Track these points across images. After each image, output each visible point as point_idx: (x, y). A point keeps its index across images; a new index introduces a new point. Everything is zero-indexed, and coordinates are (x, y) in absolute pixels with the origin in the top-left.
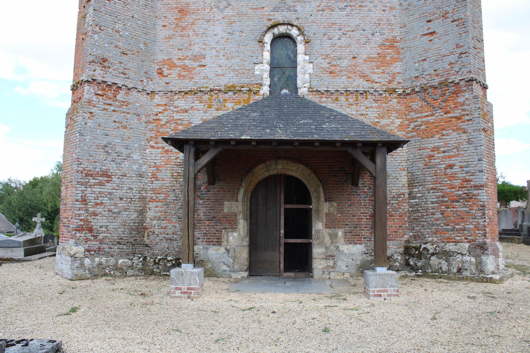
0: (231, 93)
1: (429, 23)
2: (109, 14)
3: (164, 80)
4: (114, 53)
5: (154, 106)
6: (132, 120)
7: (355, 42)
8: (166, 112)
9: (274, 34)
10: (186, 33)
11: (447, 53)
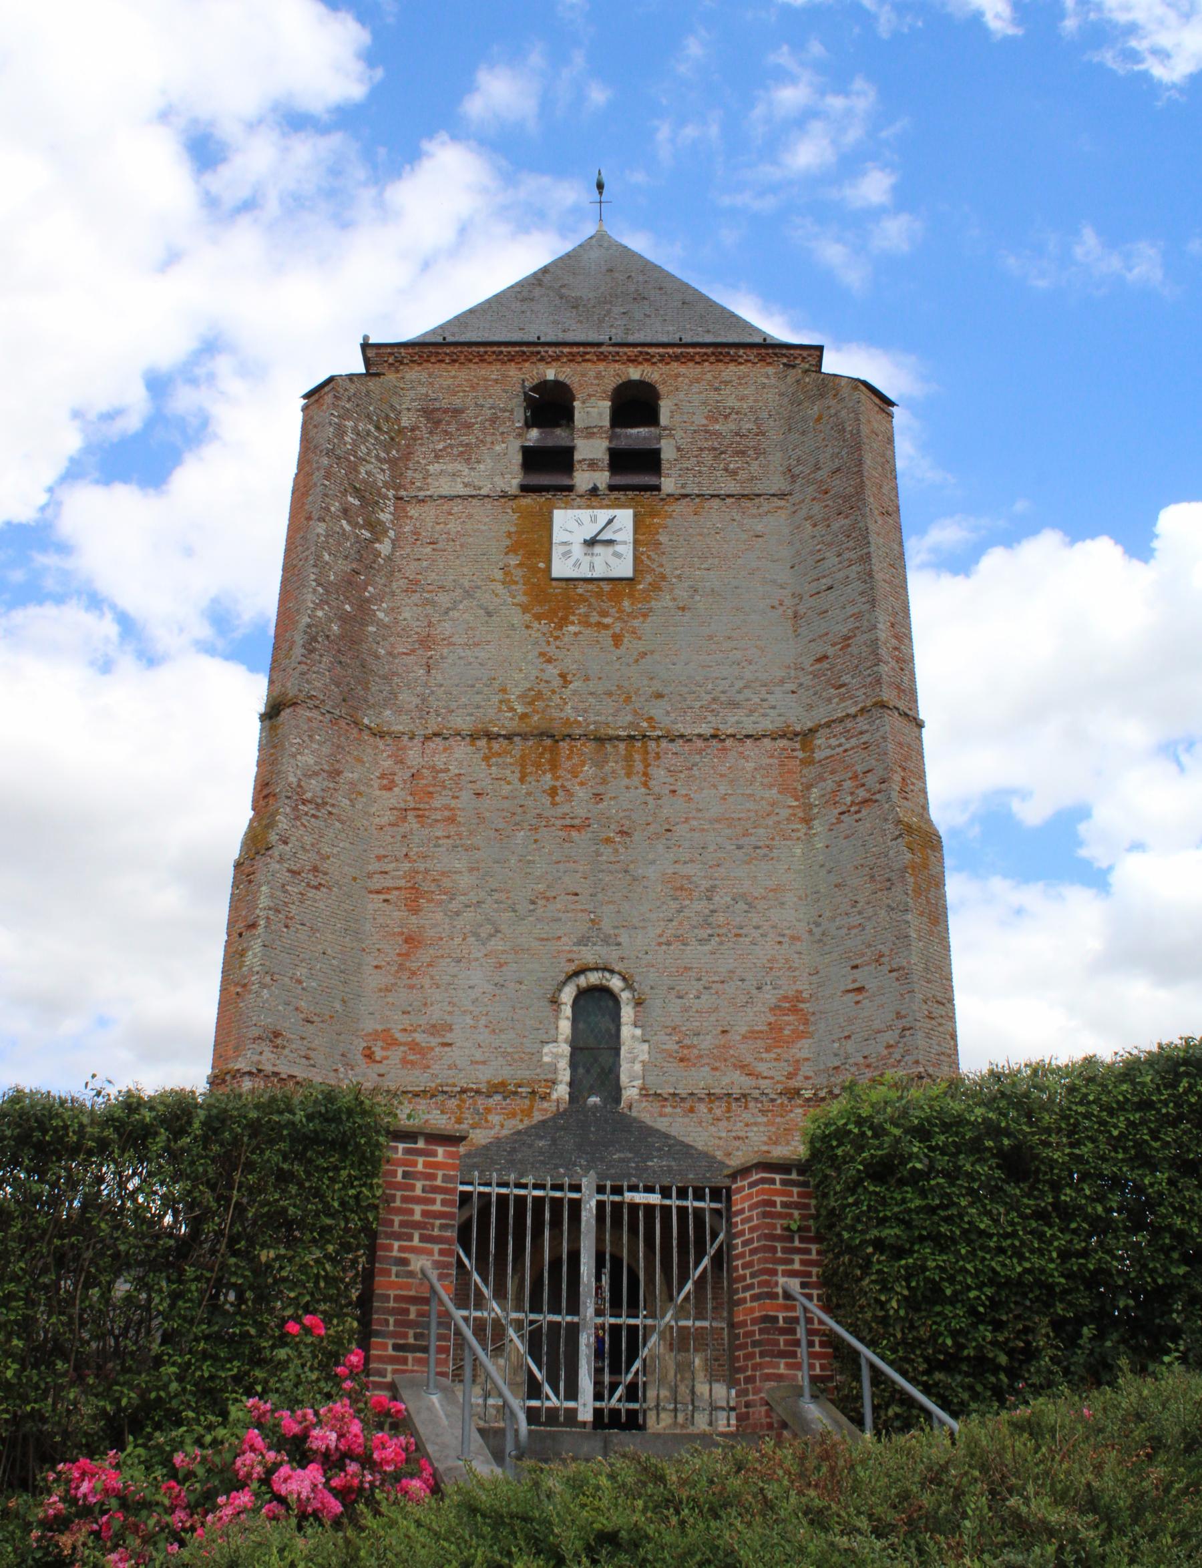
0: (498, 1097)
1: (855, 971)
9: (578, 986)
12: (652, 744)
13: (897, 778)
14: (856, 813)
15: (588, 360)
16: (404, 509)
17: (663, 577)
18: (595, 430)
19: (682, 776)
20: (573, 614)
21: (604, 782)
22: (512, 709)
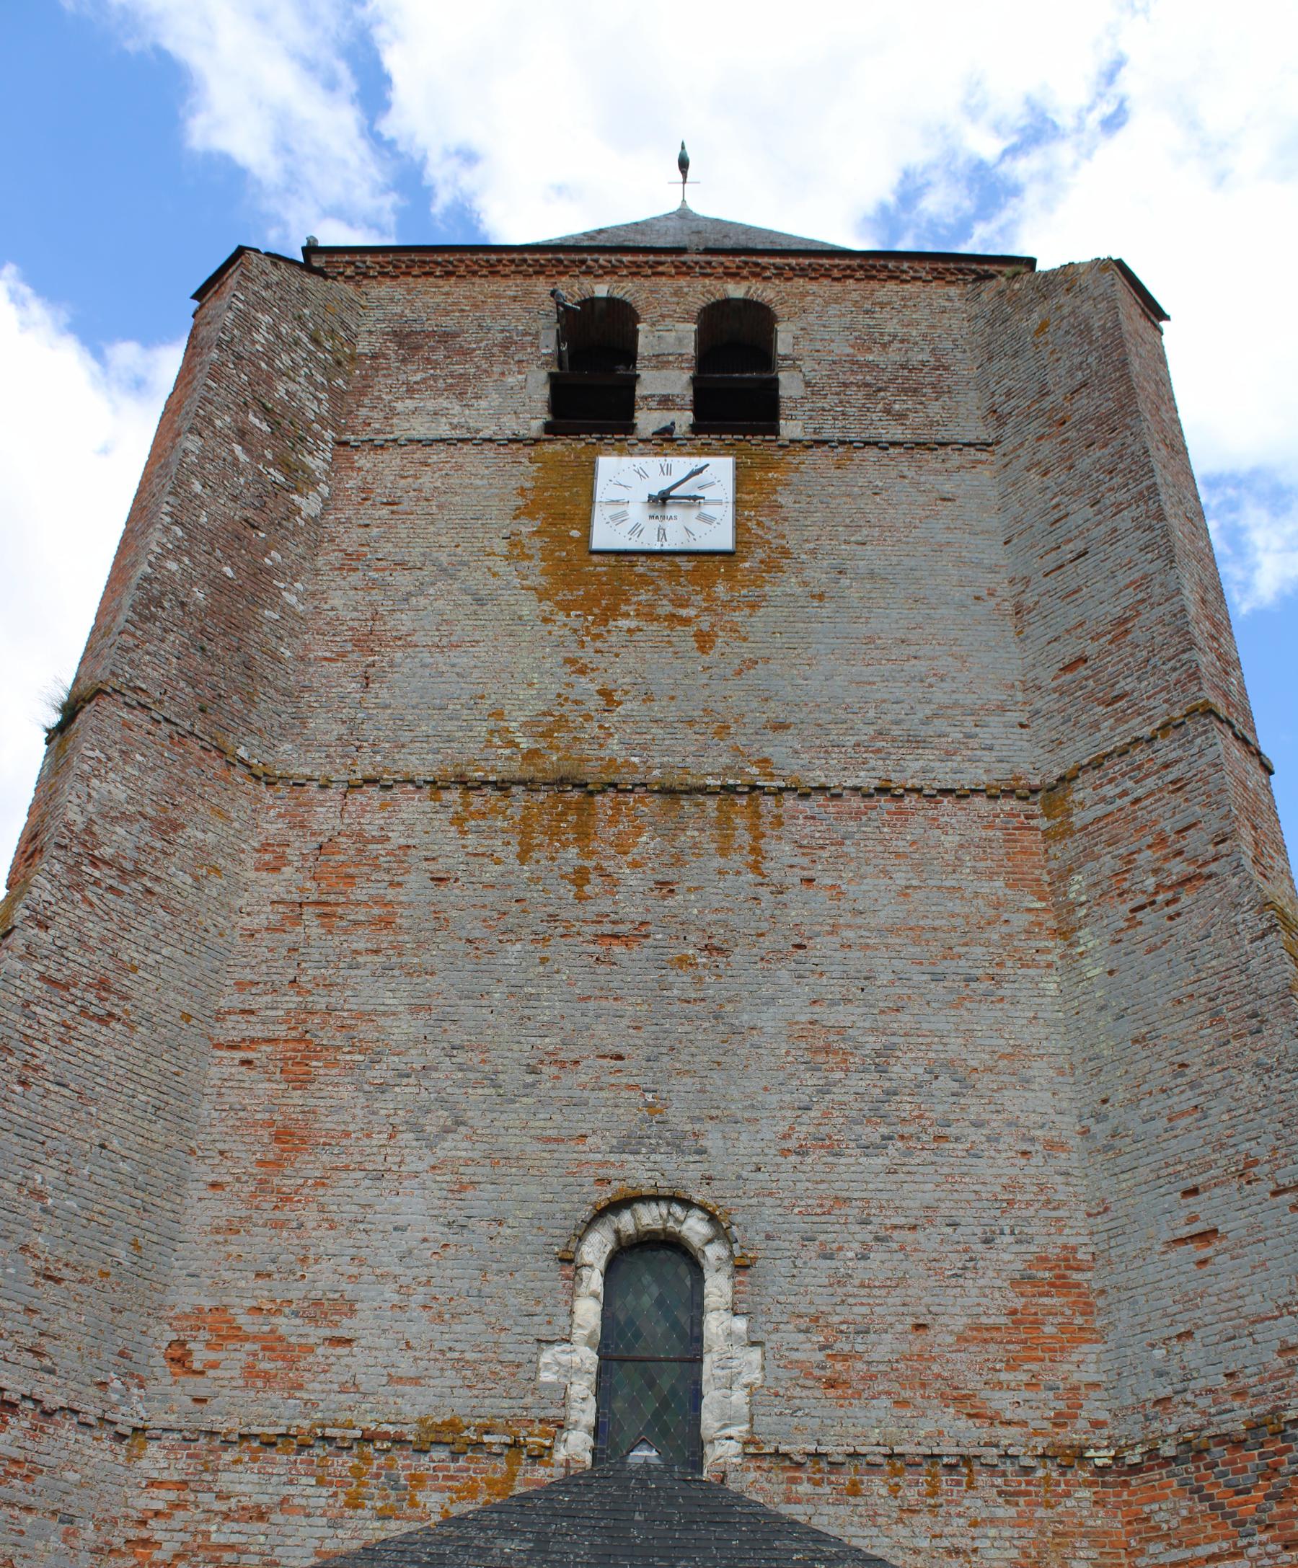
0: (440, 1454)
1: (1191, 1200)
2: (16, 1129)
3: (190, 1389)
4: (12, 1271)
5: (138, 1485)
6: (39, 1537)
7: (921, 1267)
8: (180, 1514)
9: (617, 1232)
10: (292, 1215)
11: (1268, 1308)
12: (769, 802)
13: (1246, 834)
14: (1168, 903)
15: (662, 274)
16: (349, 459)
17: (785, 553)
18: (671, 358)
19: (825, 854)
20: (627, 602)
21: (678, 861)
22: (512, 744)
